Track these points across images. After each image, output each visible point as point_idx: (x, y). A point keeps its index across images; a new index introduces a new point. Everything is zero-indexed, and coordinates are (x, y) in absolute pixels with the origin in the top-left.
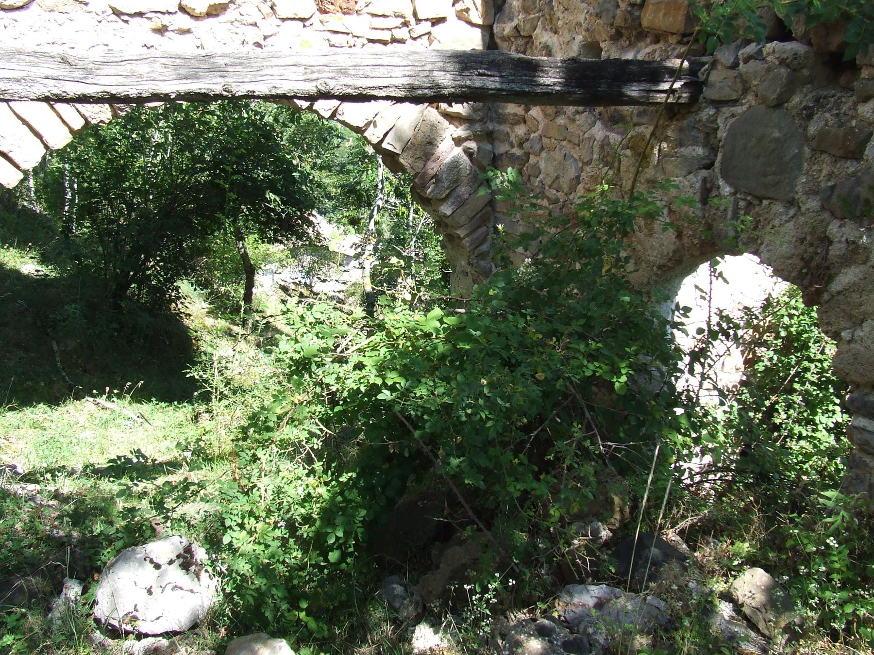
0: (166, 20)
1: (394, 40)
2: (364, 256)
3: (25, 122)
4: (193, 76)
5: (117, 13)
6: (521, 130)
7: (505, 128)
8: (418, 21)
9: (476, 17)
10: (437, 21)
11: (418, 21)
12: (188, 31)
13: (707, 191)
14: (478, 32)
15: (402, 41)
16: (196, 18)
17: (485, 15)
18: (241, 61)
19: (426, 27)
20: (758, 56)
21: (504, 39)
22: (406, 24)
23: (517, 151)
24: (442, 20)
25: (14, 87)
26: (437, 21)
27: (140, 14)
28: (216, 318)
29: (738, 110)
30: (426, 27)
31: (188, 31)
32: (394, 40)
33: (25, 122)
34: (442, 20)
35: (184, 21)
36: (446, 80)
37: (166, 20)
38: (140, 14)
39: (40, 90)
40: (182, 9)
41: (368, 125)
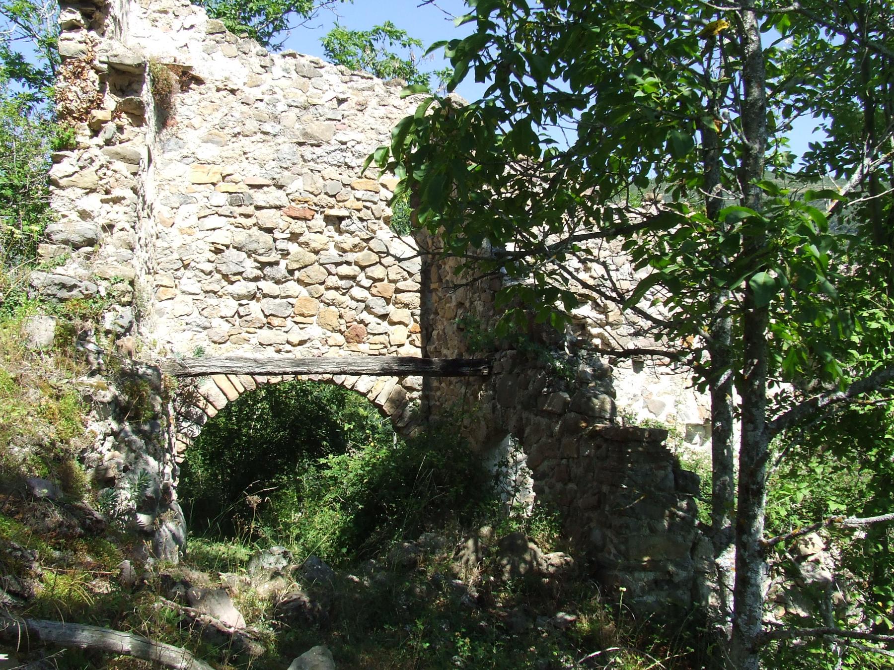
0: (281, 347)
1: (380, 354)
2: (336, 235)
3: (221, 389)
4: (298, 366)
5: (261, 344)
6: (438, 393)
7: (433, 393)
8: (391, 346)
9: (418, 343)
10: (400, 346)
11: (391, 346)
12: (290, 351)
13: (494, 408)
14: (419, 350)
15: (384, 355)
16: (294, 346)
17: (422, 343)
18: (313, 361)
19: (394, 348)
20: (505, 356)
21: (431, 353)
22: (386, 347)
23: (438, 403)
24: (403, 345)
25: (239, 369)
26: (400, 346)
27: (271, 345)
28: (399, 234)
29: (501, 376)
30: (394, 348)
31: (290, 351)
32: (380, 354)
33: (221, 389)
34: (403, 345)
35: (288, 347)
36: (395, 367)
37: (281, 347)
38: (271, 345)
39: (247, 370)
40: (288, 342)
41: (368, 392)
